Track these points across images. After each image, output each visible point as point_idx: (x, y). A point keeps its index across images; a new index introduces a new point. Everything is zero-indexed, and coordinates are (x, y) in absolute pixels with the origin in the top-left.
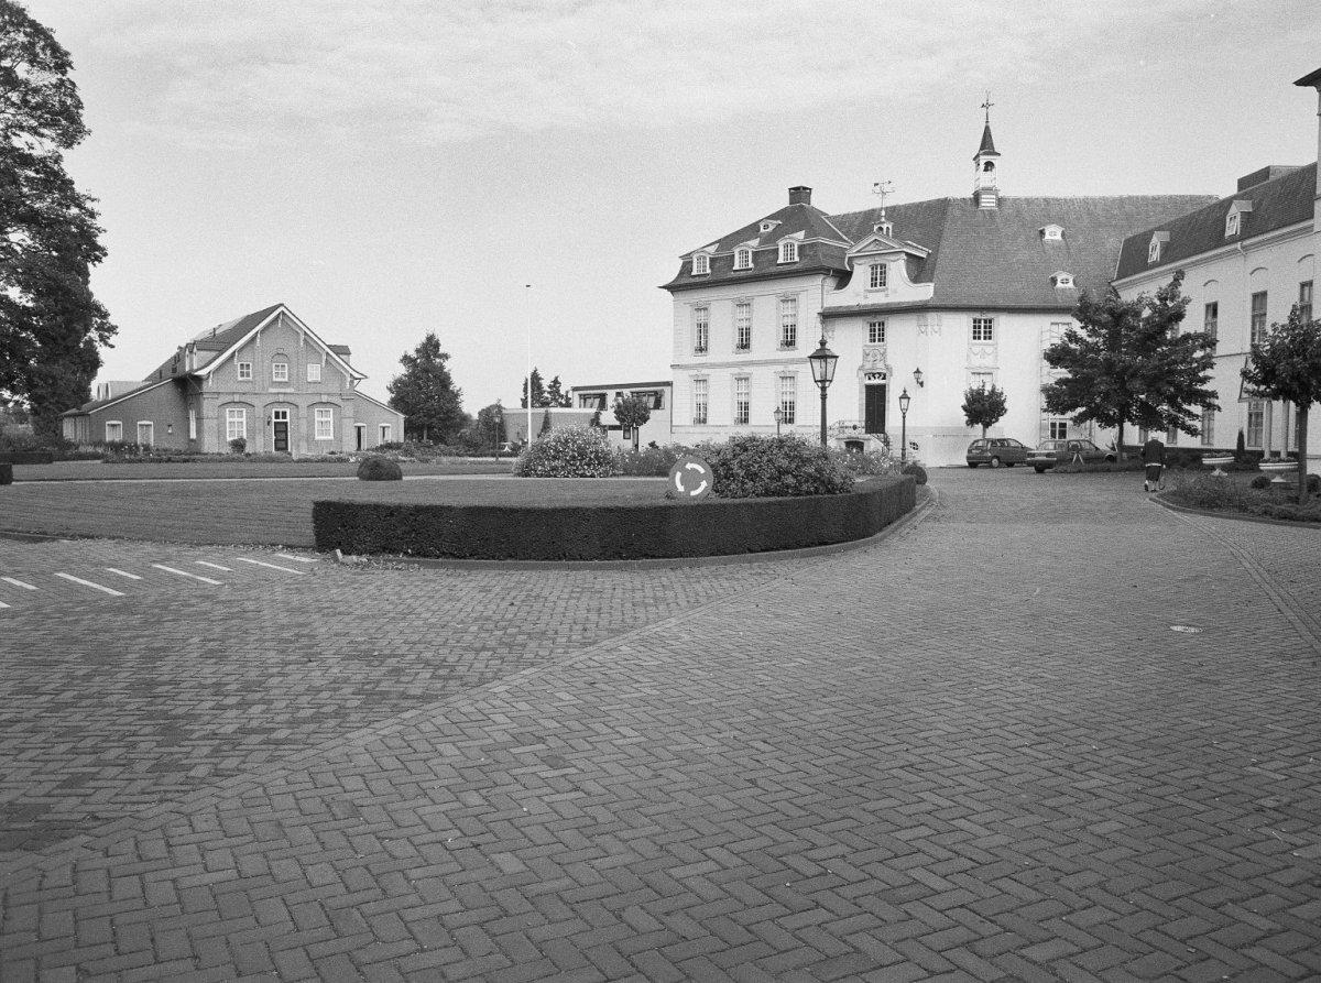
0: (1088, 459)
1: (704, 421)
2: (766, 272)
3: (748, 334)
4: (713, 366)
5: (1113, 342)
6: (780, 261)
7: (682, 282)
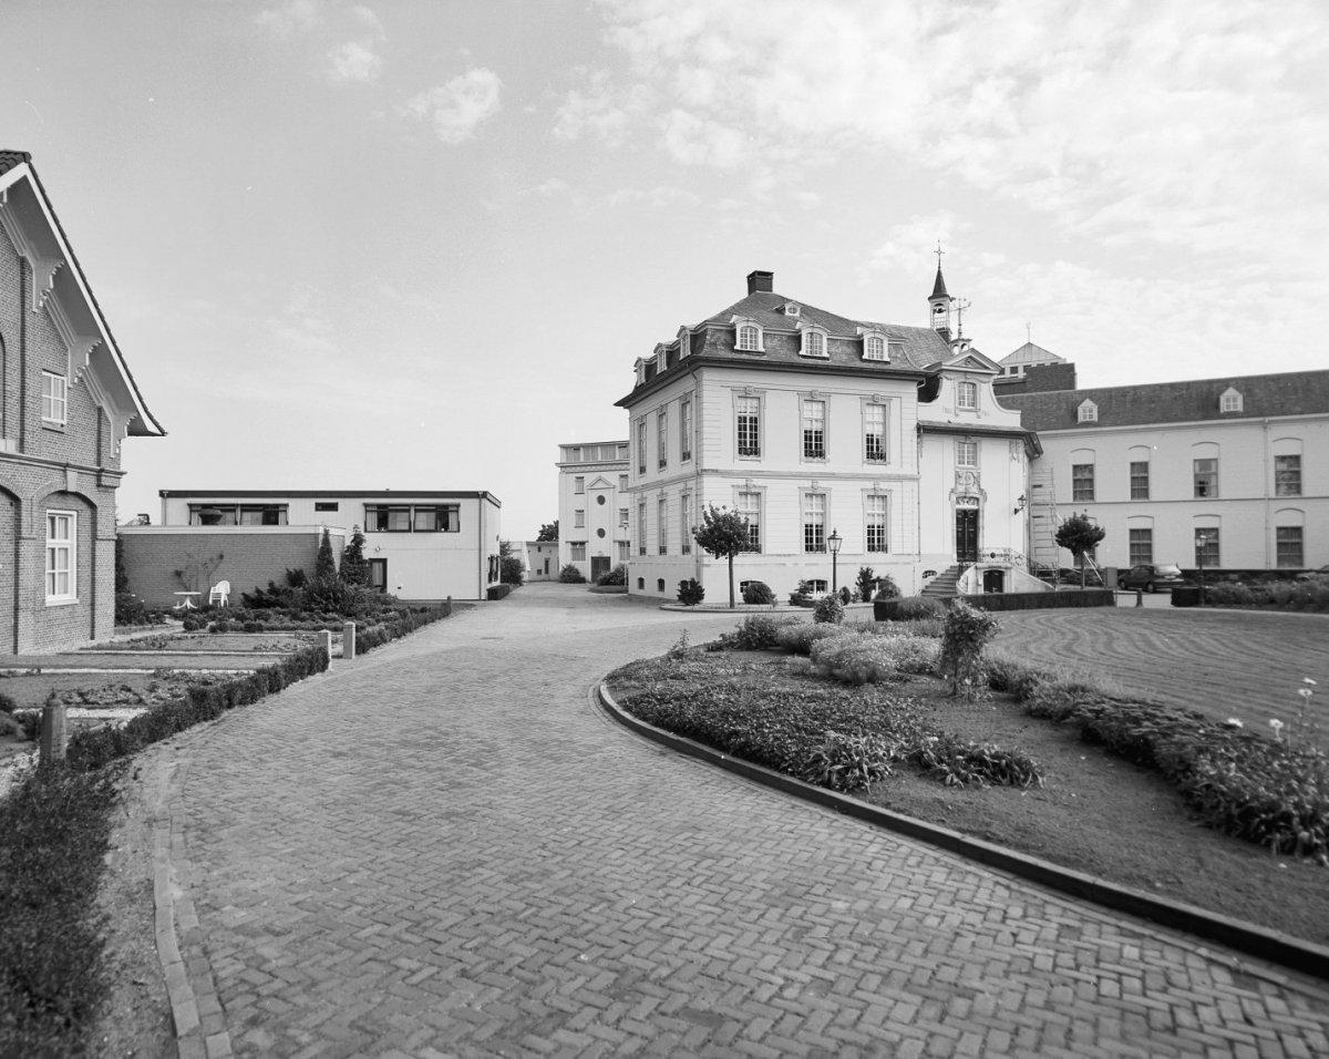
4: (900, 478)
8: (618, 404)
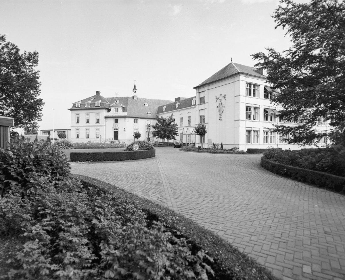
0: (159, 144)
1: (79, 138)
2: (92, 108)
3: (89, 120)
4: (101, 126)
5: (163, 125)
6: (96, 106)
7: (73, 109)
8: (193, 88)
